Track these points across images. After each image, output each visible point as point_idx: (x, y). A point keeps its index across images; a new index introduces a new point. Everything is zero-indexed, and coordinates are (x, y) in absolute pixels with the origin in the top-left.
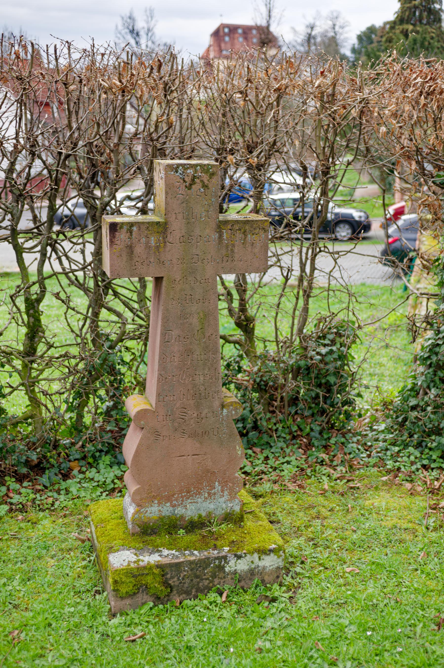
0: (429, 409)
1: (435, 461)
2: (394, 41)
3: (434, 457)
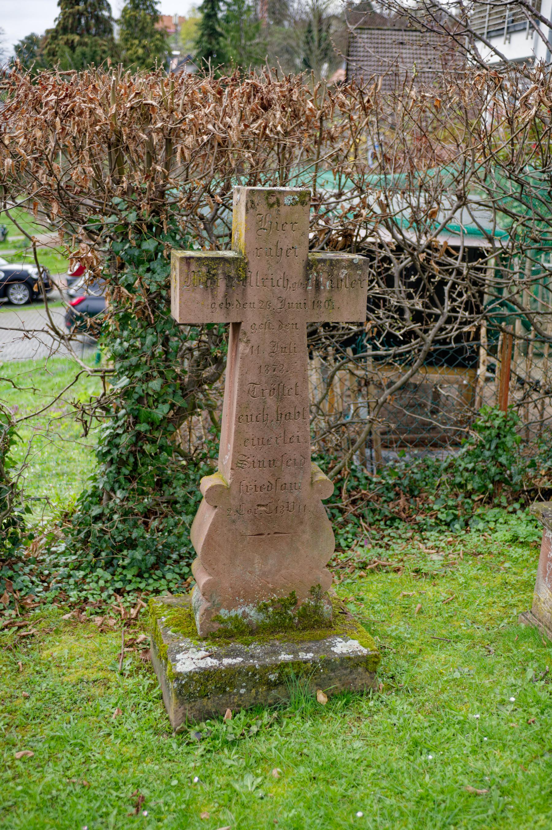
0: (116, 517)
1: (130, 581)
2: (59, 53)
3: (129, 577)
